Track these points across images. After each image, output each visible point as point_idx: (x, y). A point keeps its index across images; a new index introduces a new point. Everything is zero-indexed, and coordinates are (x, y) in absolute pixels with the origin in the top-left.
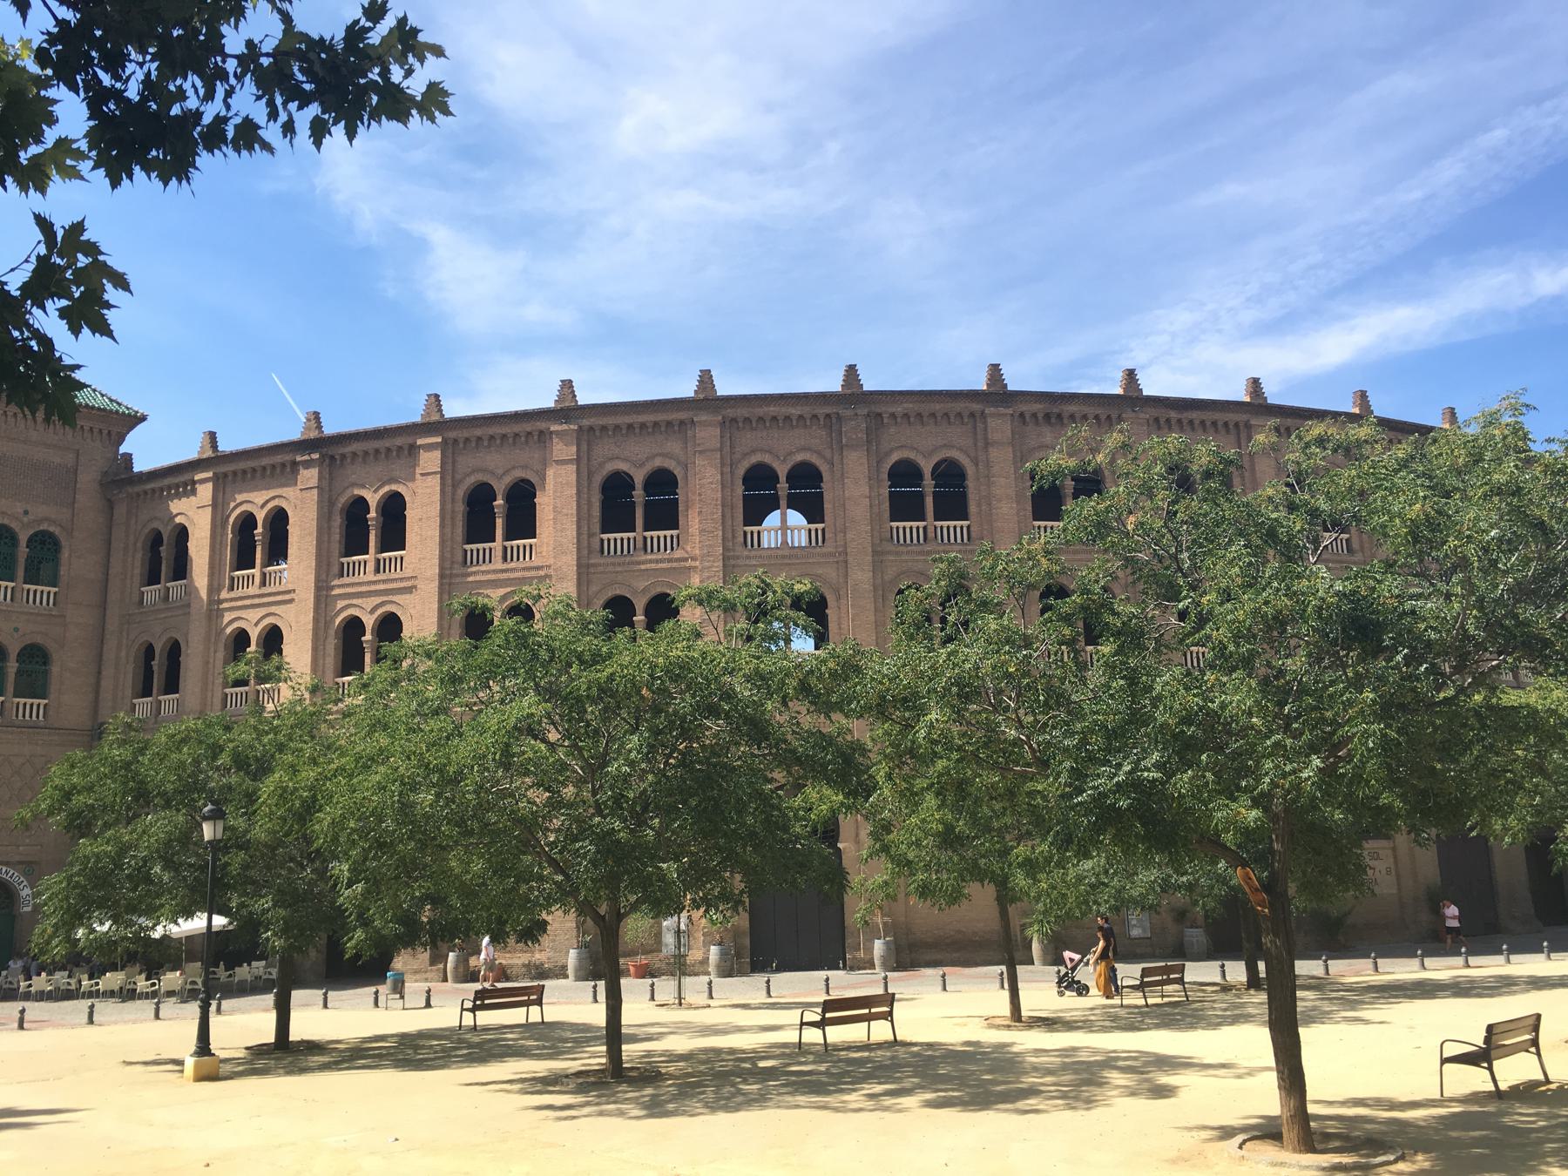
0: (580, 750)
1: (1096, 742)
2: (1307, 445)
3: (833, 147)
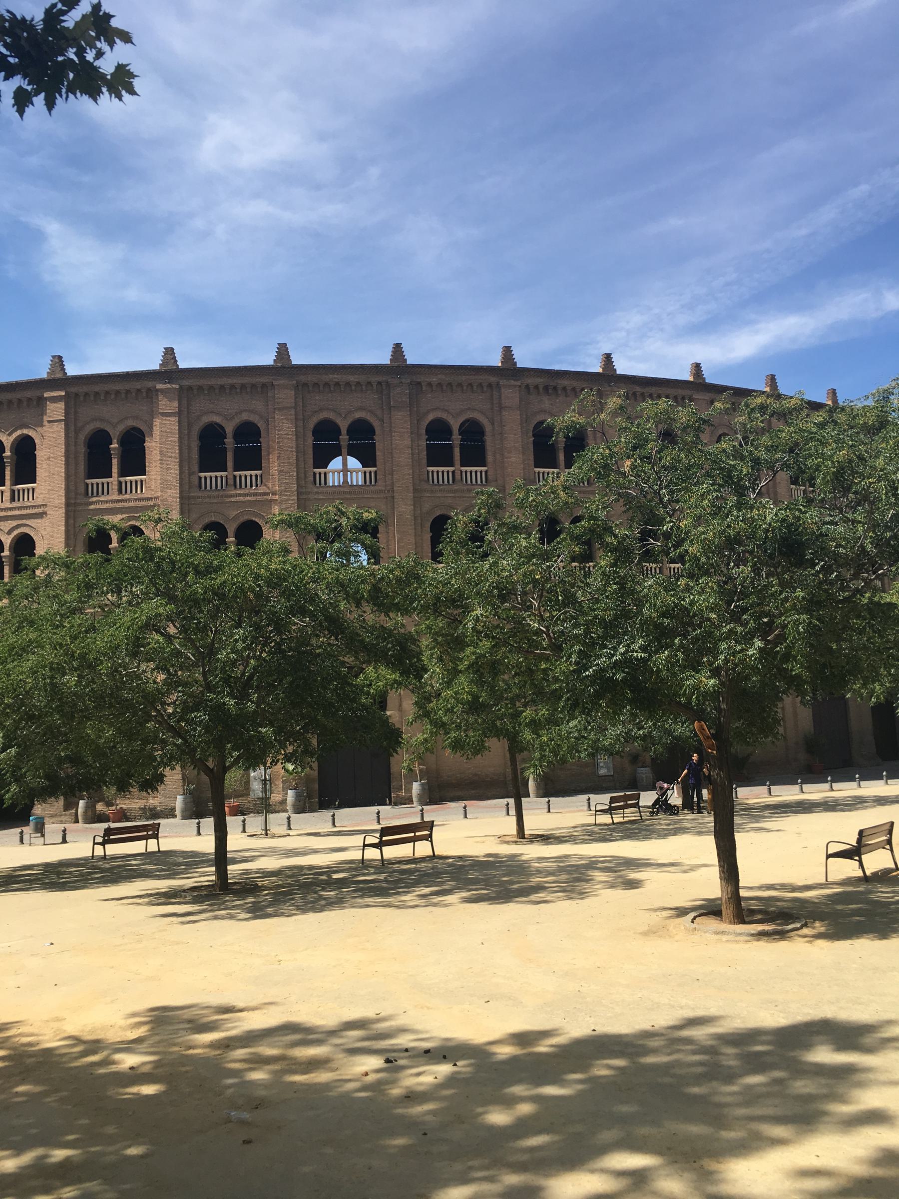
0: (192, 641)
1: (597, 632)
2: (752, 410)
3: (374, 172)
